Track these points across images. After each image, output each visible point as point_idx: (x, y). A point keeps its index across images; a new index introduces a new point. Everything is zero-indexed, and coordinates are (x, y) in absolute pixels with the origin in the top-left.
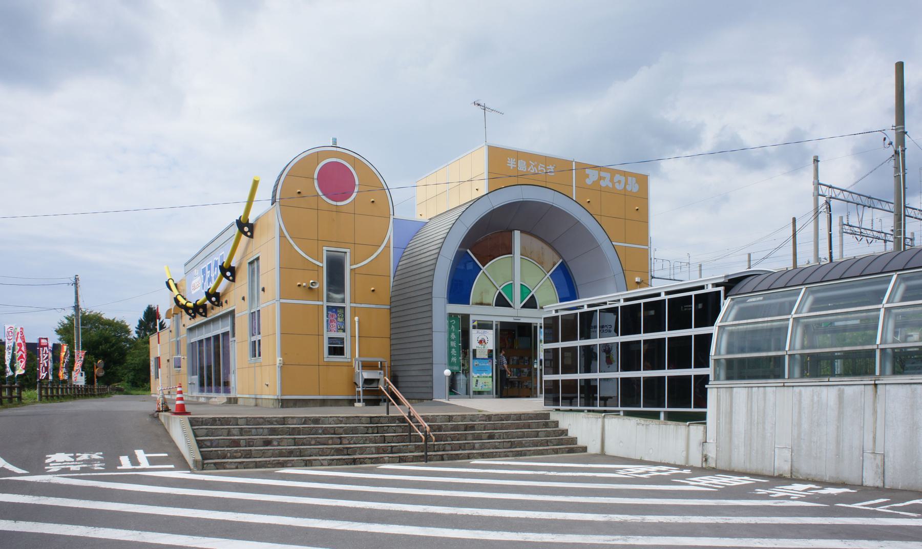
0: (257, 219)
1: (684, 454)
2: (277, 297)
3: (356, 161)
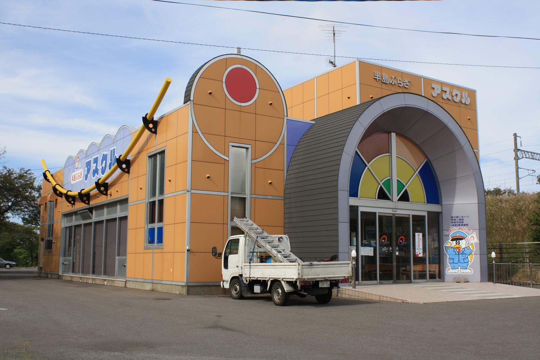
0: (162, 118)
1: (199, 288)
2: (188, 187)
3: (257, 67)
